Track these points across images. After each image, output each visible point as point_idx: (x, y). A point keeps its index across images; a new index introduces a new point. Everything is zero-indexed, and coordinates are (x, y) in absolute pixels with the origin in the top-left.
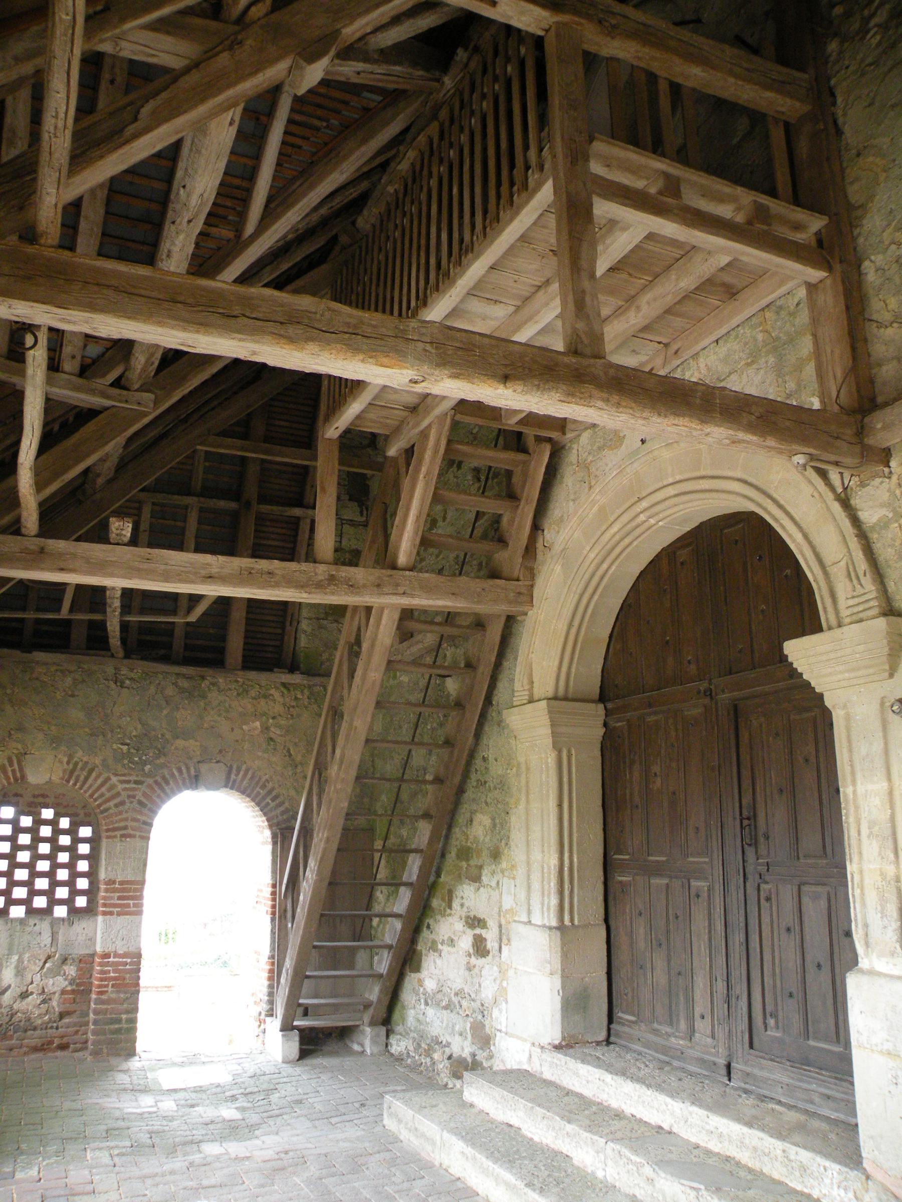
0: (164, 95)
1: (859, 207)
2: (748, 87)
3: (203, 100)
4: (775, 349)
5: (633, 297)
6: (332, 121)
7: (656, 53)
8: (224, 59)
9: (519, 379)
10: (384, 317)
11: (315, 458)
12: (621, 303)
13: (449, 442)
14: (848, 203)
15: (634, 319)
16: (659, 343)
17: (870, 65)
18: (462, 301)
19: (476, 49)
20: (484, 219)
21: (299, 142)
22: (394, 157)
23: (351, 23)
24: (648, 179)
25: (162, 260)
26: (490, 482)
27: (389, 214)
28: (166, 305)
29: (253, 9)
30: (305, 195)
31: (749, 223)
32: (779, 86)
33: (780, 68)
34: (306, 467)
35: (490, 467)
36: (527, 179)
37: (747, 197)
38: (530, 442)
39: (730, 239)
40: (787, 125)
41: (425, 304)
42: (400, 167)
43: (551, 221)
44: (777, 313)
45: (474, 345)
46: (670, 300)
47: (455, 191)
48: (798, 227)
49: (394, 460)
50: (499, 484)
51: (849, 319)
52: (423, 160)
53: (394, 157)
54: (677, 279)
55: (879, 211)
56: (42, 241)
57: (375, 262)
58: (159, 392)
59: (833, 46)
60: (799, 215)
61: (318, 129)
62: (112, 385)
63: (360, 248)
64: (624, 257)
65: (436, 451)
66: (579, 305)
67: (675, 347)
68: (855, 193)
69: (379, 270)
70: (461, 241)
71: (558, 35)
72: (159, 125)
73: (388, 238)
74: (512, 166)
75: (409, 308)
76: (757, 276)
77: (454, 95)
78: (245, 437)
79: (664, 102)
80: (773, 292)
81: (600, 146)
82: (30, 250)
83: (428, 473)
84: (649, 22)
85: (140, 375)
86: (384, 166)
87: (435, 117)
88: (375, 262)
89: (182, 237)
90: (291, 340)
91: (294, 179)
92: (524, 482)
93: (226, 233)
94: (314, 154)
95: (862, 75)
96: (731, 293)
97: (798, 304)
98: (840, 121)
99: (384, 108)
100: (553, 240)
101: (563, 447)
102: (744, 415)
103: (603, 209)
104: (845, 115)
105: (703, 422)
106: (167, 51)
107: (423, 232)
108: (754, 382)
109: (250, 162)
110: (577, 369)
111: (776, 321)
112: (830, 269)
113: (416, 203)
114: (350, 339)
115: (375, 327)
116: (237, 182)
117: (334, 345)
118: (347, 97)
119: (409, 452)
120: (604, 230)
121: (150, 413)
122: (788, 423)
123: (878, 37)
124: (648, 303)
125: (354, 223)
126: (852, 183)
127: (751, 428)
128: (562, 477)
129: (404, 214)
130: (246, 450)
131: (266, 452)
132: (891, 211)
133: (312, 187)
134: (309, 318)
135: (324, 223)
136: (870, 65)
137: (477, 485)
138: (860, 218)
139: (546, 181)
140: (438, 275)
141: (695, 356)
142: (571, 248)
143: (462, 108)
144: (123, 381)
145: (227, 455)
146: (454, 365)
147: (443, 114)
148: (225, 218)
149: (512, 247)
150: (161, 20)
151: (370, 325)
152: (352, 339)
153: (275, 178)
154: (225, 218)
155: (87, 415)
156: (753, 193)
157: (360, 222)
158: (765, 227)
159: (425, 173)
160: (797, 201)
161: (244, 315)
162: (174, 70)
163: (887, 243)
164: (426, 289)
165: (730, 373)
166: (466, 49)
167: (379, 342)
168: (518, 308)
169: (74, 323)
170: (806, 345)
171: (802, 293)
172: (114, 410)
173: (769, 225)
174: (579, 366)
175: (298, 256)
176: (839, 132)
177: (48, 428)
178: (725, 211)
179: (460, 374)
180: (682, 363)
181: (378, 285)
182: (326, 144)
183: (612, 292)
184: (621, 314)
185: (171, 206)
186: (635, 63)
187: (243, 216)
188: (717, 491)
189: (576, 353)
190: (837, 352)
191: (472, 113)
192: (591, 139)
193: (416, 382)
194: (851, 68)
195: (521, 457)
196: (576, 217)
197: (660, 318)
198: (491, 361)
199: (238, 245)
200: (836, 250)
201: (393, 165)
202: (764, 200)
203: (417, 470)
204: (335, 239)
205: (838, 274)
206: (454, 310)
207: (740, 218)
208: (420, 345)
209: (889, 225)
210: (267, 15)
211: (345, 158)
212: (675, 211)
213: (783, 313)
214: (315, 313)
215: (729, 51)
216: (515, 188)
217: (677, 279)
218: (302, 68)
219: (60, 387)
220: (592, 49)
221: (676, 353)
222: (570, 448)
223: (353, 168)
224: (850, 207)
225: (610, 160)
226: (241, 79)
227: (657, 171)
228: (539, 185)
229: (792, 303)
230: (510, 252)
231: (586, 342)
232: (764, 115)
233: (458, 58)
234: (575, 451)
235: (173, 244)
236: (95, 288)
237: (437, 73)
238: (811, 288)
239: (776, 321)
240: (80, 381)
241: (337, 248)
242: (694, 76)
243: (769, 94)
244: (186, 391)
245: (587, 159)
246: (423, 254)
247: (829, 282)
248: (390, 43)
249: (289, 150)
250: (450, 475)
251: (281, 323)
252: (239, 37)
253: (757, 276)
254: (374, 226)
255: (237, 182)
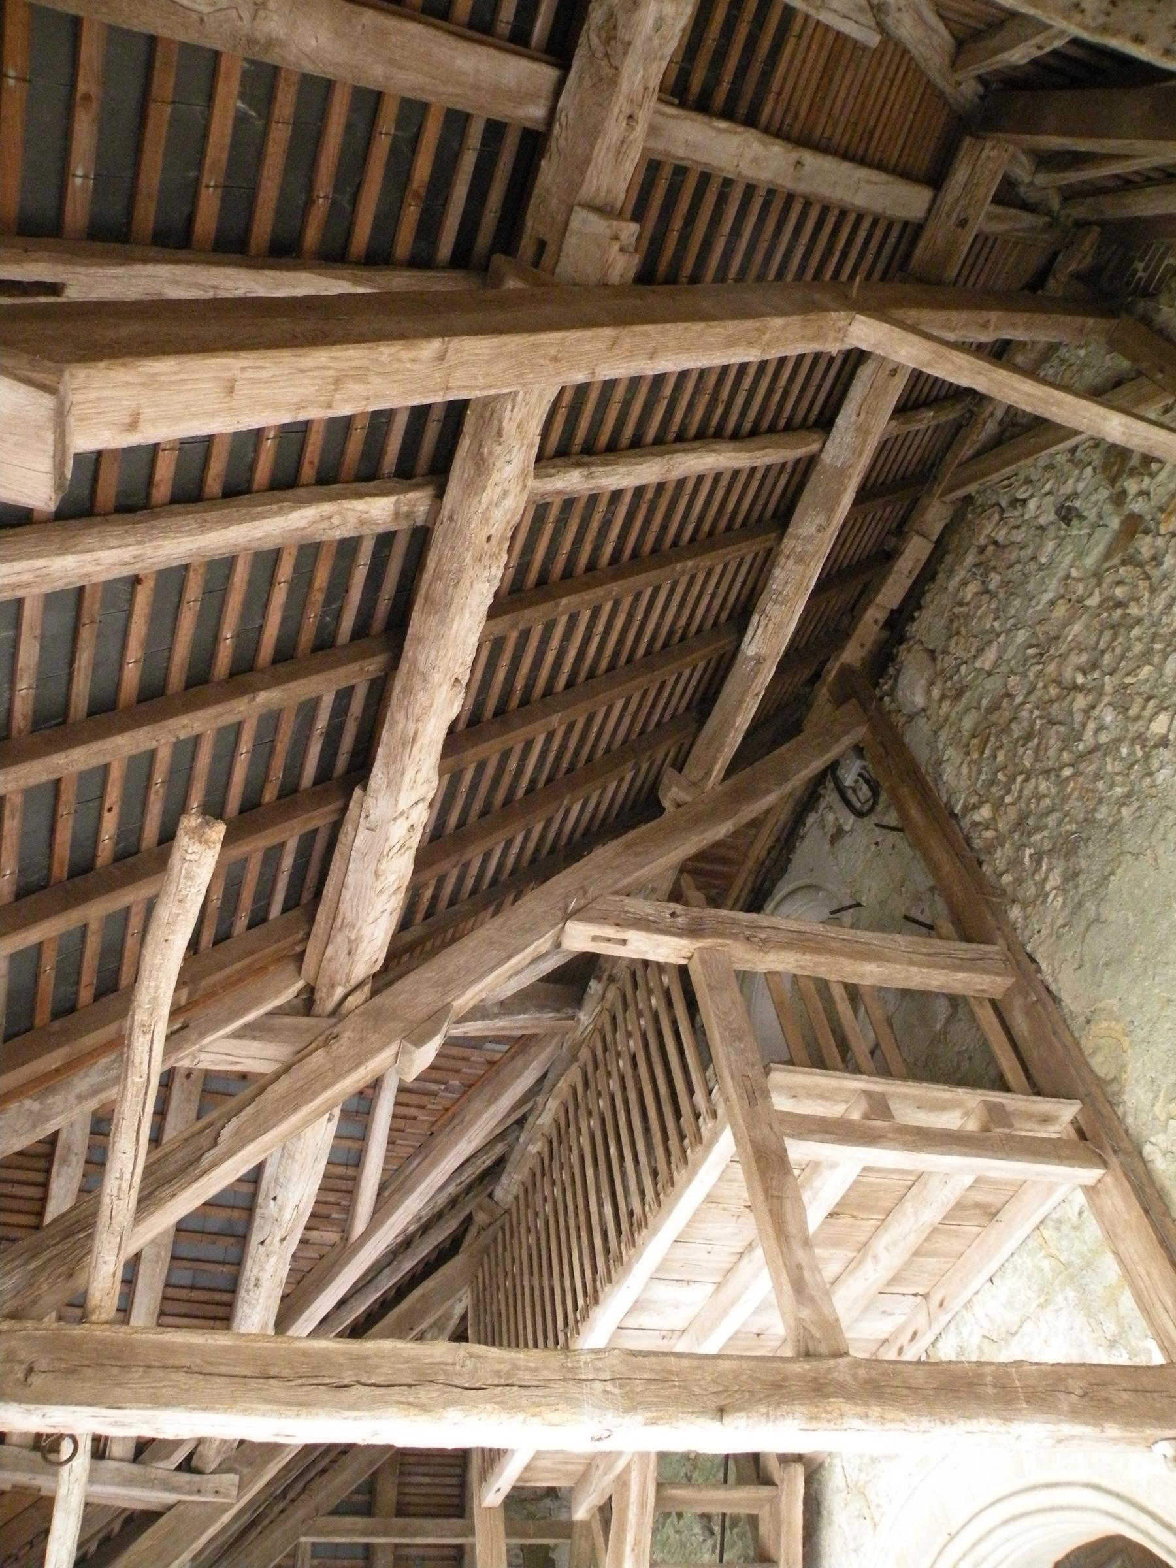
0: (249, 1110)
1: (1113, 1080)
2: (935, 972)
3: (296, 1108)
4: (1071, 1278)
5: (866, 1244)
6: (452, 1082)
7: (818, 958)
8: (319, 1057)
9: (740, 1409)
10: (546, 1353)
11: (470, 1531)
12: (851, 1255)
13: (659, 1486)
14: (1098, 1078)
15: (874, 1273)
16: (915, 1295)
17: (1064, 926)
18: (646, 1288)
19: (612, 979)
20: (655, 1183)
21: (413, 1112)
22: (532, 1110)
23: (464, 993)
24: (847, 1102)
25: (248, 1291)
26: (728, 1533)
27: (535, 1185)
28: (253, 1384)
29: (350, 999)
30: (425, 1175)
31: (986, 1129)
32: (970, 965)
33: (964, 945)
34: (460, 1548)
35: (724, 1515)
36: (698, 1128)
37: (973, 1098)
38: (774, 1467)
39: (965, 1155)
40: (993, 1003)
41: (596, 1301)
42: (540, 1121)
43: (738, 1171)
44: (1058, 1229)
45: (670, 1372)
46: (914, 1240)
47: (613, 1150)
48: (1046, 1119)
49: (586, 1524)
50: (742, 1535)
51: (1154, 1225)
52: (567, 1111)
53: (532, 1110)
54: (916, 1213)
55: (1137, 1081)
56: (94, 1318)
57: (524, 1247)
58: (245, 1471)
59: (1015, 912)
60: (1044, 1105)
61: (434, 1094)
62: (179, 1468)
63: (503, 1228)
64: (843, 1197)
65: (643, 1505)
66: (799, 1285)
67: (936, 1298)
68: (1101, 1065)
69: (530, 1257)
70: (631, 1214)
71: (703, 962)
72: (243, 1146)
73: (536, 1214)
74: (678, 1115)
75: (576, 1308)
76: (1016, 1188)
77: (594, 1030)
78: (368, 1510)
79: (843, 1008)
80: (1042, 1205)
81: (780, 1077)
82: (78, 1331)
83: (637, 1542)
84: (803, 929)
85: (218, 1452)
86: (521, 1122)
87: (575, 1058)
88: (524, 1247)
89: (273, 1260)
90: (423, 1408)
91: (410, 1157)
92: (778, 1535)
93: (332, 1236)
94: (434, 1123)
95: (1059, 937)
96: (991, 1213)
97: (1080, 1213)
98: (1053, 988)
99: (513, 1058)
100: (746, 1195)
101: (821, 1465)
102: (1061, 1396)
103: (798, 1151)
104: (1056, 980)
105: (1006, 1420)
106: (256, 1057)
107: (581, 1206)
108: (1058, 1338)
109: (355, 1145)
110: (815, 1379)
111: (1060, 1239)
112: (1105, 1164)
113: (566, 1167)
114: (502, 1393)
115: (535, 1370)
116: (340, 1170)
117: (482, 1407)
118: (467, 1052)
119: (605, 1511)
120: (808, 1170)
121: (232, 1505)
122: (1126, 1396)
123: (1060, 899)
124: (886, 1249)
125: (490, 1196)
126: (1093, 1054)
127: (1075, 1414)
128: (830, 1513)
129: (554, 1183)
130: (372, 1534)
131: (402, 1533)
132: (1153, 1080)
133: (434, 1164)
134: (445, 1373)
135: (453, 1202)
136: (1064, 926)
137: (710, 1542)
138: (1120, 1093)
139: (723, 1128)
140: (607, 1260)
141: (968, 1305)
142: (770, 1211)
143: (605, 1050)
144: (195, 1462)
145: (343, 1544)
146: (648, 1406)
147: (584, 1054)
148: (328, 1217)
149: (697, 1213)
150: (246, 1026)
151: (527, 1369)
152: (505, 1389)
153: (387, 1160)
154: (328, 1217)
155: (138, 1521)
156: (979, 1091)
157: (499, 1193)
158: (1007, 1130)
159: (572, 1129)
160: (1037, 1091)
161: (359, 1383)
162: (264, 1075)
163: (1162, 1118)
164: (594, 1281)
165: (1022, 1323)
166: (599, 980)
167: (541, 1392)
168: (719, 1286)
169: (130, 1425)
170: (1110, 1268)
171: (1080, 1198)
172: (182, 1507)
173: (1011, 1126)
174: (817, 1371)
175: (425, 1248)
176: (1056, 1000)
177: (83, 1550)
178: (951, 1120)
179: (658, 1419)
180: (953, 1318)
181: (531, 1274)
182: (447, 1110)
183: (836, 1242)
184: (856, 1268)
185: (258, 1211)
186: (799, 972)
187: (349, 1211)
188: (1062, 1508)
189: (808, 1355)
190: (1156, 1274)
191: (619, 1055)
192: (767, 1071)
193: (599, 1439)
194: (1044, 932)
195: (765, 1491)
196: (769, 1168)
197: (908, 1264)
198: (697, 1390)
199: (346, 1250)
200: (1100, 1137)
201: (530, 1119)
202: (995, 1097)
203: (621, 1541)
204: (469, 1219)
205: (1118, 1169)
206: (636, 1302)
207: (972, 1126)
208: (598, 1386)
209: (1156, 1097)
210: (366, 1001)
211: (472, 1123)
212: (890, 1135)
213: (1065, 1228)
214: (454, 1364)
215: (902, 940)
216: (686, 1141)
217: (916, 1213)
218: (410, 1053)
219: (104, 1483)
220: (747, 967)
221: (941, 1305)
222: (831, 1465)
223: (483, 1134)
224: (1101, 1082)
225: (797, 1092)
226: (340, 1077)
227: (855, 1091)
228: (716, 1135)
229: (1072, 1212)
230: (696, 1218)
231: (818, 1335)
232: (964, 997)
233: (591, 991)
234: (838, 1470)
235: (262, 1269)
236: (161, 1373)
237: (570, 1011)
238: (1090, 1191)
239: (1060, 1239)
240: (135, 1469)
241: (473, 1230)
242: (868, 973)
243: (960, 976)
244: (260, 291)
245: (766, 1094)
246: (583, 1233)
247: (1109, 1180)
248: (510, 993)
249: (401, 1123)
250: (669, 1530)
251: (410, 1386)
252: (335, 1030)
253: (1016, 1188)
254: (517, 1198)
255: (340, 1170)
